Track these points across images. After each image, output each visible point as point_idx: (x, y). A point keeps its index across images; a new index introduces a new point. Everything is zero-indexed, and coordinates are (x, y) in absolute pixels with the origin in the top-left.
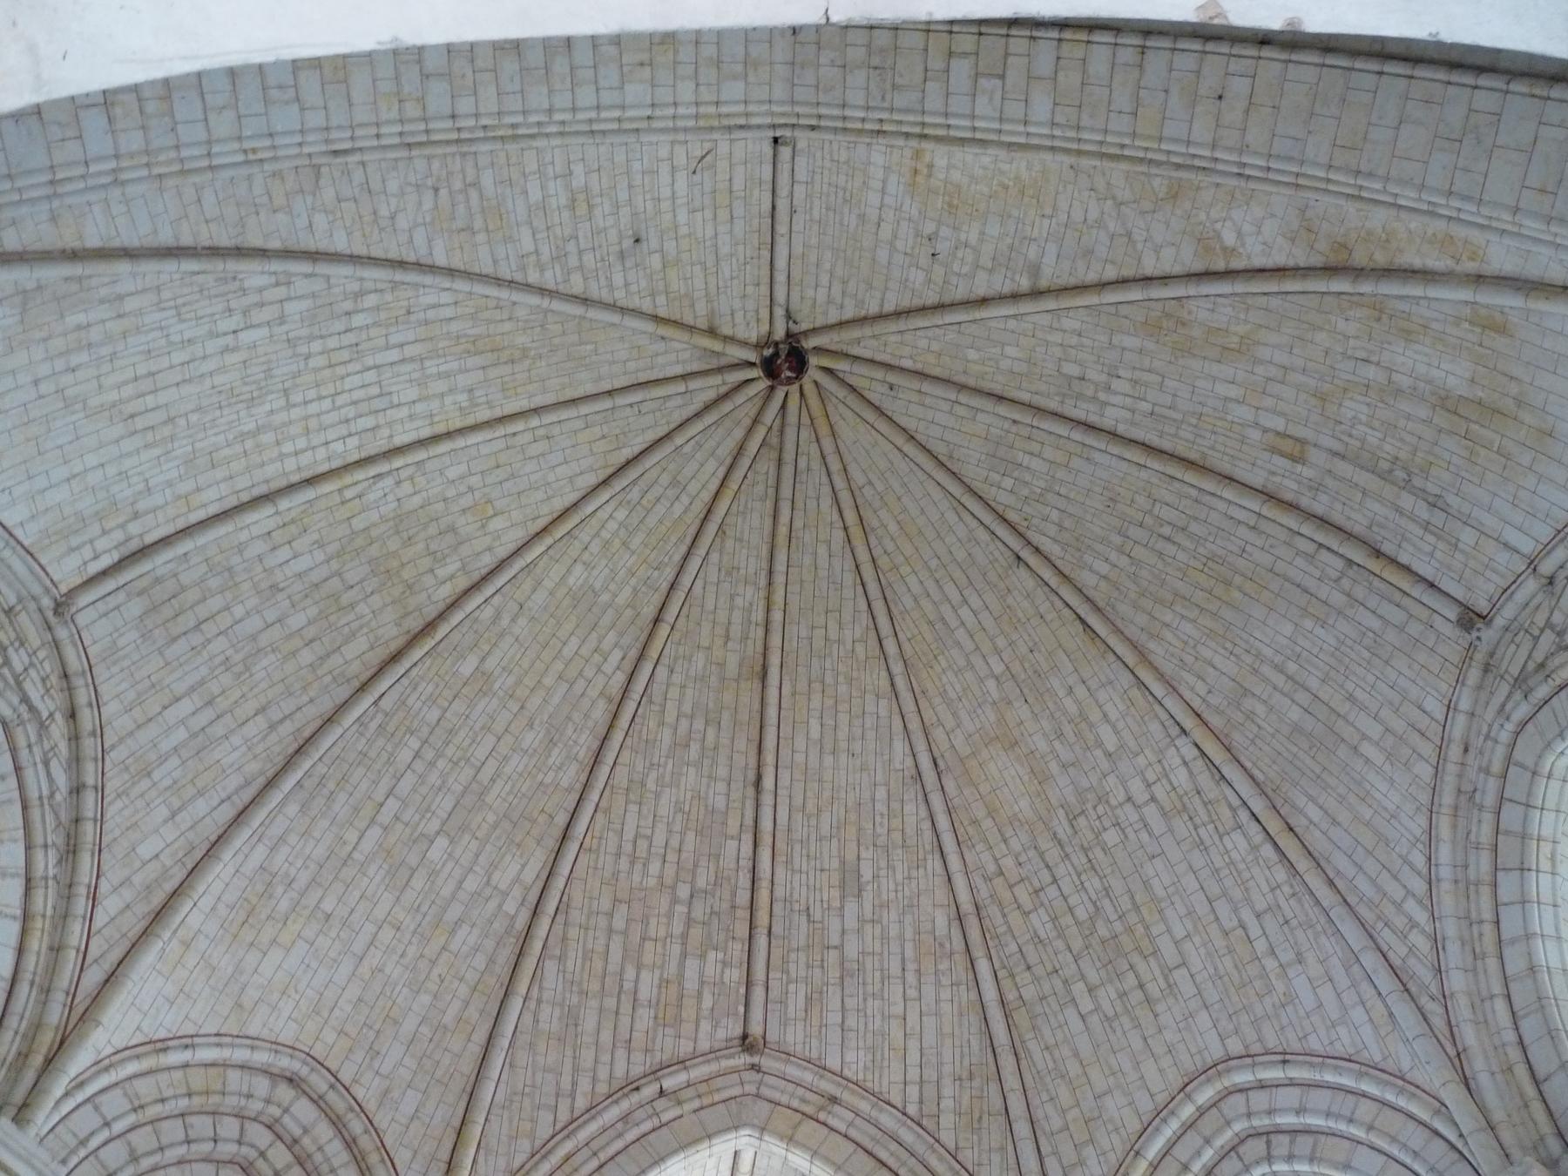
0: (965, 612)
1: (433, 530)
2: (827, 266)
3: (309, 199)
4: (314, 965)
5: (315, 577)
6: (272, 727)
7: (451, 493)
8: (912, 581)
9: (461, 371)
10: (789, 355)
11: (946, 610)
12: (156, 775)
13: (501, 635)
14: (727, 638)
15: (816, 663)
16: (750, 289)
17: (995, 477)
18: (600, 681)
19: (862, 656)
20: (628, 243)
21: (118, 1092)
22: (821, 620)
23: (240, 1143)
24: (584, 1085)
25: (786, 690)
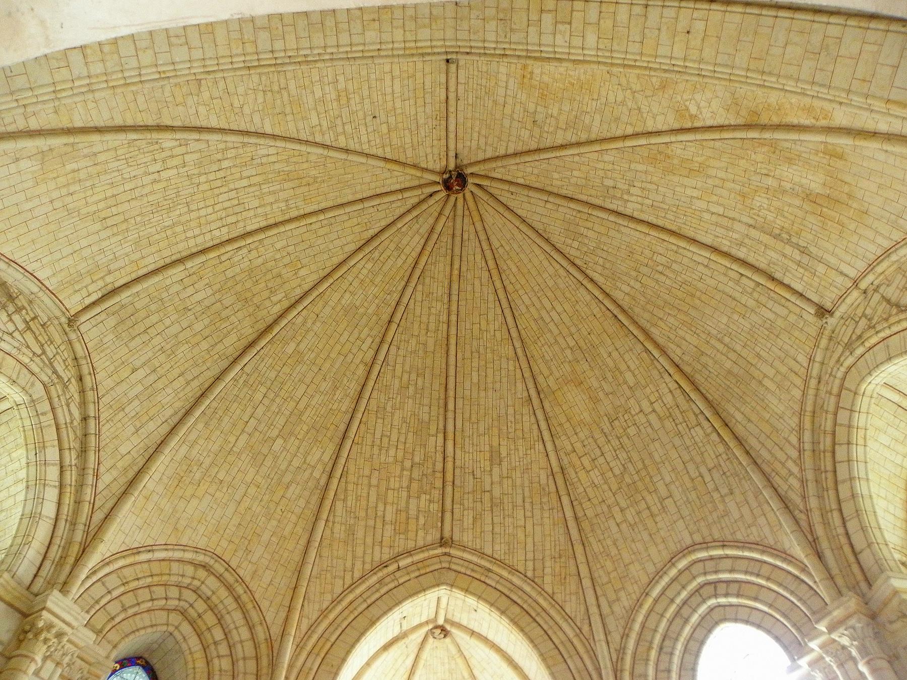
0: (553, 314)
1: (269, 276)
2: (477, 129)
3: (196, 98)
4: (215, 506)
5: (207, 303)
6: (188, 383)
7: (278, 256)
8: (525, 297)
9: (281, 190)
12: (127, 410)
15: (475, 343)
16: (435, 142)
18: (360, 355)
21: (114, 576)
23: (179, 600)
24: (358, 565)
25: (460, 355)
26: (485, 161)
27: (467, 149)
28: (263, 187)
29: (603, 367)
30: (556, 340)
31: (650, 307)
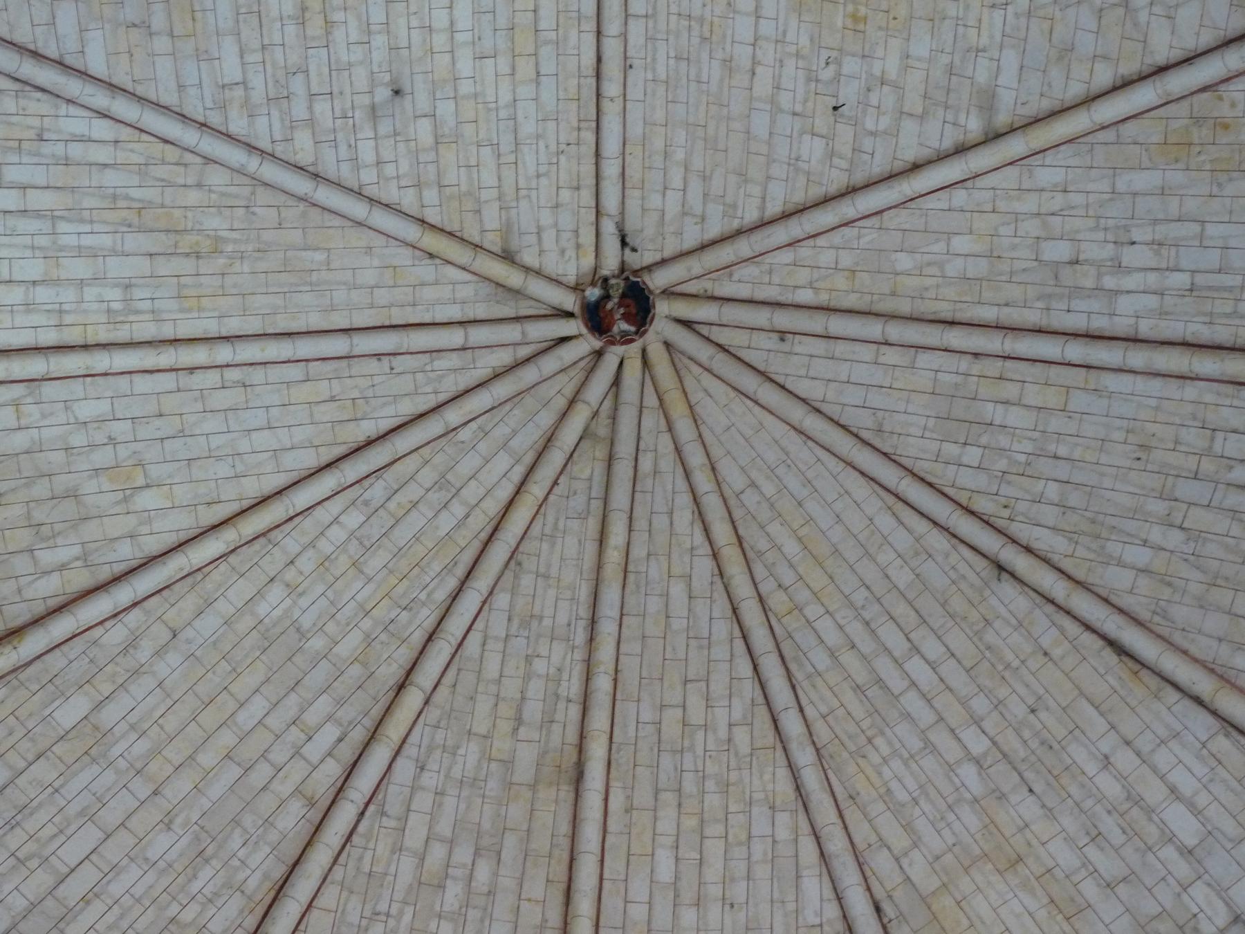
0: (916, 667)
1: (41, 489)
2: (680, 155)
7: (78, 440)
8: (825, 626)
9: (114, 253)
10: (623, 296)
11: (884, 667)
13: (136, 673)
14: (519, 721)
15: (667, 762)
16: (565, 195)
17: (951, 449)
18: (297, 771)
19: (745, 749)
20: (383, 94)
22: (674, 696)
25: (616, 802)
26: (703, 247)
27: (655, 217)
28: (63, 227)
29: (1089, 803)
30: (928, 743)
31: (1223, 597)
